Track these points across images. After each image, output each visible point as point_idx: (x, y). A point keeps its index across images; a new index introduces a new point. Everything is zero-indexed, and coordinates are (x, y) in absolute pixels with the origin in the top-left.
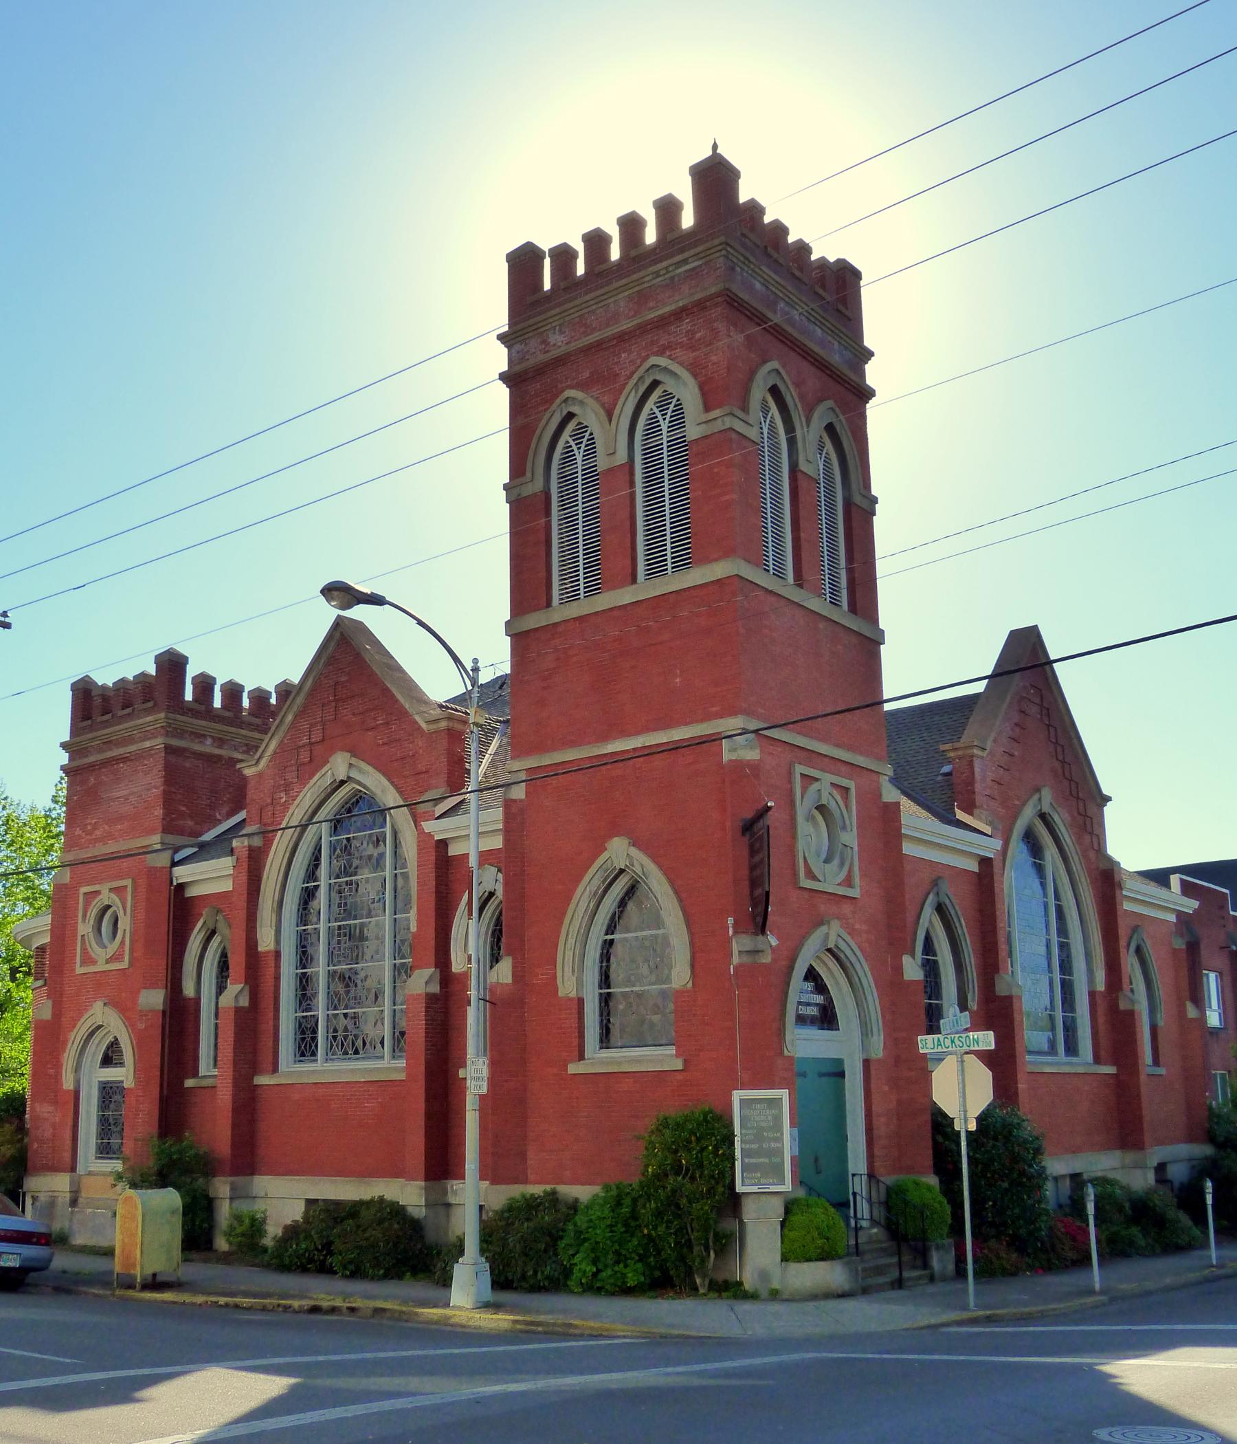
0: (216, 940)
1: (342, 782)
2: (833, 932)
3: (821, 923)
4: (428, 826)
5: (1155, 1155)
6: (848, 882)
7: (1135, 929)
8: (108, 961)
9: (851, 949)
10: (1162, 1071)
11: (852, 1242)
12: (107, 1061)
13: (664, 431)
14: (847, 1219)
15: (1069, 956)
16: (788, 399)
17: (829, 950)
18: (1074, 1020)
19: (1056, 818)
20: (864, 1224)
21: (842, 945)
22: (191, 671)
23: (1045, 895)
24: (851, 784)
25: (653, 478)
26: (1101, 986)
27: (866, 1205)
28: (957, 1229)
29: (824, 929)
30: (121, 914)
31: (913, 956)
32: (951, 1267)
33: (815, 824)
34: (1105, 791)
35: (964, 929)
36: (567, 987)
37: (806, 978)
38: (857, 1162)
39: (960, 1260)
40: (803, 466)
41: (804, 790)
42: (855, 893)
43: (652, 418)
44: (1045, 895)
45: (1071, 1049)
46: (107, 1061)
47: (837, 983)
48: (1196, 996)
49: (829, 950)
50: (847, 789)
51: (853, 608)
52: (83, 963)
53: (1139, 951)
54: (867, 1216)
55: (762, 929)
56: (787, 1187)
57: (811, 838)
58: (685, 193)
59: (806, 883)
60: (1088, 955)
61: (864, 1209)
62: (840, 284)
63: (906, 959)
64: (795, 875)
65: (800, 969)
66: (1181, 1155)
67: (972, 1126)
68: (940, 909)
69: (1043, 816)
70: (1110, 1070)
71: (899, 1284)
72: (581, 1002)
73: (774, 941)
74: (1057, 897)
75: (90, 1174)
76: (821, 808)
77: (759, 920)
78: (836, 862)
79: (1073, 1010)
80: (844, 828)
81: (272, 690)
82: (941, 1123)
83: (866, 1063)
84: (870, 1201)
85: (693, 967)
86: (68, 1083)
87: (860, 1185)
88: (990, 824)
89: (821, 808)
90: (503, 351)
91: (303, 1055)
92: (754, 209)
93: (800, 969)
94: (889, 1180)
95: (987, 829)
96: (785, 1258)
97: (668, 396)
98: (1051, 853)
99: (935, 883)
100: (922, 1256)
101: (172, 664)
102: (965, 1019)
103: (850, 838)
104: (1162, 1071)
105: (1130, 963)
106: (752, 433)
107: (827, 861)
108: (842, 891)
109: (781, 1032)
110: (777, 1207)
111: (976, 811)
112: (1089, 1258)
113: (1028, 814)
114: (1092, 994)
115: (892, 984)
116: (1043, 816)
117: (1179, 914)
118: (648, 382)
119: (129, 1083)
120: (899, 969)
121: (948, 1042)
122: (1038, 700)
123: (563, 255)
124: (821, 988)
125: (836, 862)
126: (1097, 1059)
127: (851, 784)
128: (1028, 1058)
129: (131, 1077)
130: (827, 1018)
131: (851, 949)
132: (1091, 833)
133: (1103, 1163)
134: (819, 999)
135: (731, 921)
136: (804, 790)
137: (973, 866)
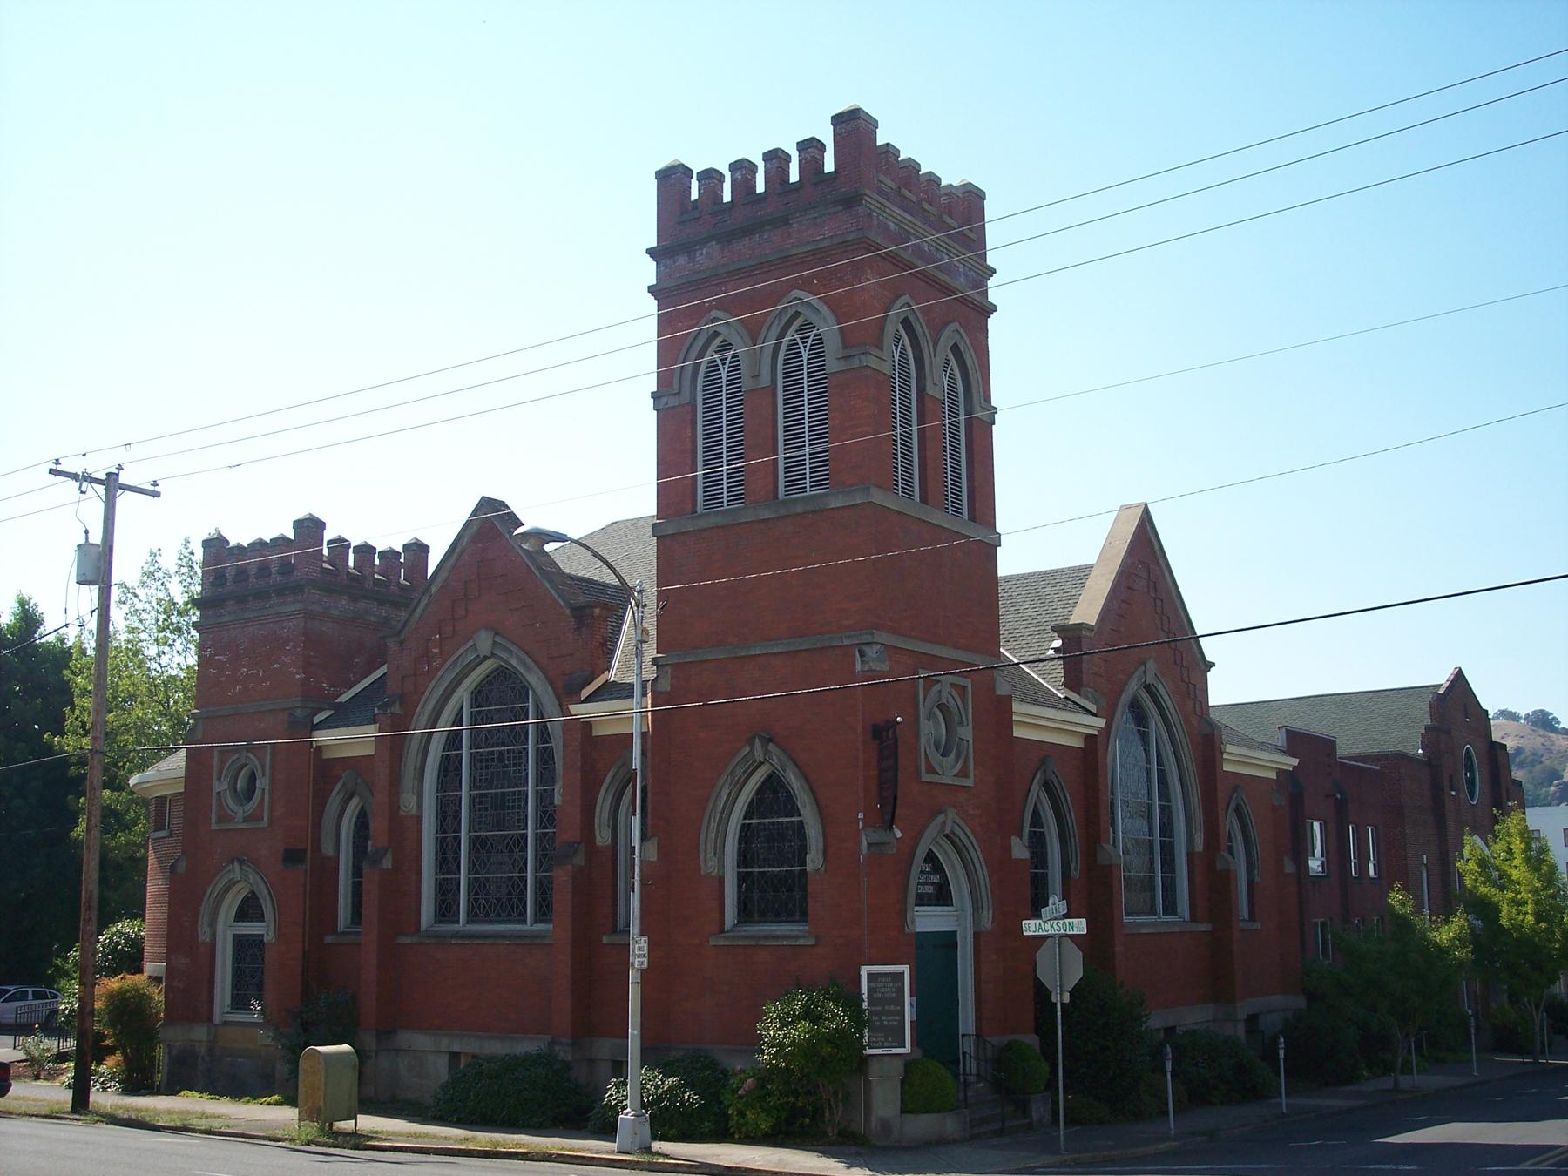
0: (355, 802)
1: (486, 658)
2: (950, 819)
3: (940, 812)
4: (580, 710)
5: (1244, 1009)
6: (963, 773)
7: (1235, 789)
8: (245, 820)
9: (966, 835)
10: (1258, 926)
11: (961, 1096)
12: (242, 915)
13: (805, 358)
14: (956, 1076)
15: (1170, 818)
16: (918, 330)
17: (946, 836)
18: (1173, 880)
19: (1160, 688)
20: (972, 1079)
21: (957, 830)
22: (328, 535)
23: (1148, 761)
24: (968, 683)
25: (793, 395)
26: (1199, 845)
27: (974, 1065)
28: (1051, 1085)
29: (941, 818)
30: (259, 774)
31: (1021, 837)
32: (1048, 1118)
33: (937, 722)
34: (1209, 658)
35: (1068, 803)
36: (709, 866)
37: (925, 861)
38: (967, 1021)
39: (1055, 1114)
40: (930, 390)
41: (927, 691)
42: (969, 782)
43: (793, 343)
44: (1148, 761)
45: (1170, 908)
46: (242, 915)
47: (953, 866)
48: (1300, 852)
49: (946, 836)
50: (964, 687)
51: (972, 518)
52: (219, 821)
53: (1238, 810)
54: (974, 1071)
55: (890, 827)
56: (907, 1049)
57: (931, 730)
58: (827, 136)
59: (926, 777)
60: (1188, 824)
61: (972, 1067)
62: (970, 202)
63: (1015, 840)
64: (918, 771)
65: (921, 854)
66: (1277, 1006)
67: (1067, 998)
68: (1047, 785)
69: (1147, 688)
70: (1204, 927)
71: (1000, 1133)
72: (721, 880)
73: (899, 834)
74: (1160, 762)
75: (226, 1023)
76: (943, 708)
77: (888, 817)
78: (952, 756)
79: (1173, 871)
80: (961, 723)
81: (400, 550)
82: (1042, 993)
83: (977, 935)
84: (977, 1059)
85: (825, 852)
86: (204, 935)
87: (967, 1046)
88: (1095, 702)
89: (943, 708)
90: (652, 265)
91: (443, 915)
92: (890, 151)
93: (921, 854)
94: (996, 1040)
95: (1093, 708)
96: (904, 1111)
97: (807, 326)
98: (1155, 722)
99: (1043, 761)
100: (1023, 1108)
101: (310, 527)
102: (1062, 907)
103: (966, 732)
104: (1258, 926)
105: (1230, 823)
106: (886, 369)
107: (943, 755)
108: (957, 782)
109: (902, 914)
110: (899, 1065)
111: (1083, 690)
112: (1166, 1113)
113: (1133, 686)
114: (1190, 855)
115: (1000, 863)
116: (1147, 688)
117: (1280, 772)
118: (791, 312)
119: (269, 938)
120: (1008, 849)
121: (1048, 927)
122: (1145, 575)
123: (711, 178)
124: (938, 868)
125: (952, 756)
126: (1193, 919)
127: (968, 683)
128: (1126, 919)
129: (271, 933)
130: (942, 896)
131: (966, 835)
132: (1194, 699)
133: (1194, 1017)
134: (936, 879)
135: (861, 815)
136: (927, 691)
137: (1077, 743)
